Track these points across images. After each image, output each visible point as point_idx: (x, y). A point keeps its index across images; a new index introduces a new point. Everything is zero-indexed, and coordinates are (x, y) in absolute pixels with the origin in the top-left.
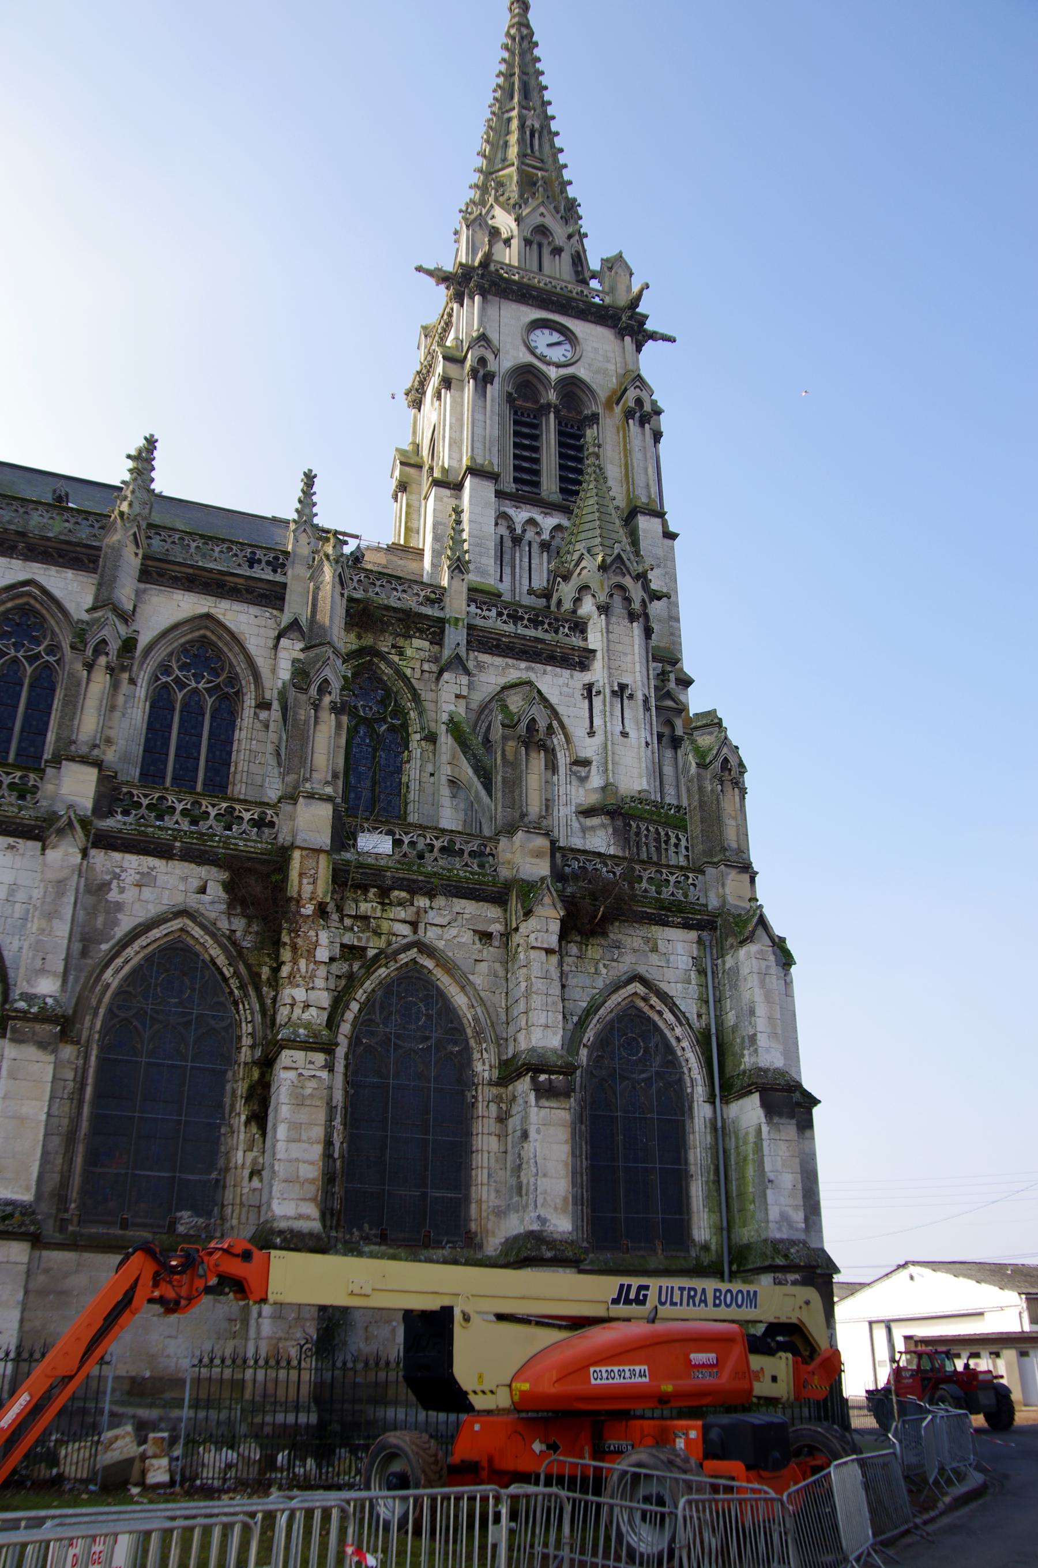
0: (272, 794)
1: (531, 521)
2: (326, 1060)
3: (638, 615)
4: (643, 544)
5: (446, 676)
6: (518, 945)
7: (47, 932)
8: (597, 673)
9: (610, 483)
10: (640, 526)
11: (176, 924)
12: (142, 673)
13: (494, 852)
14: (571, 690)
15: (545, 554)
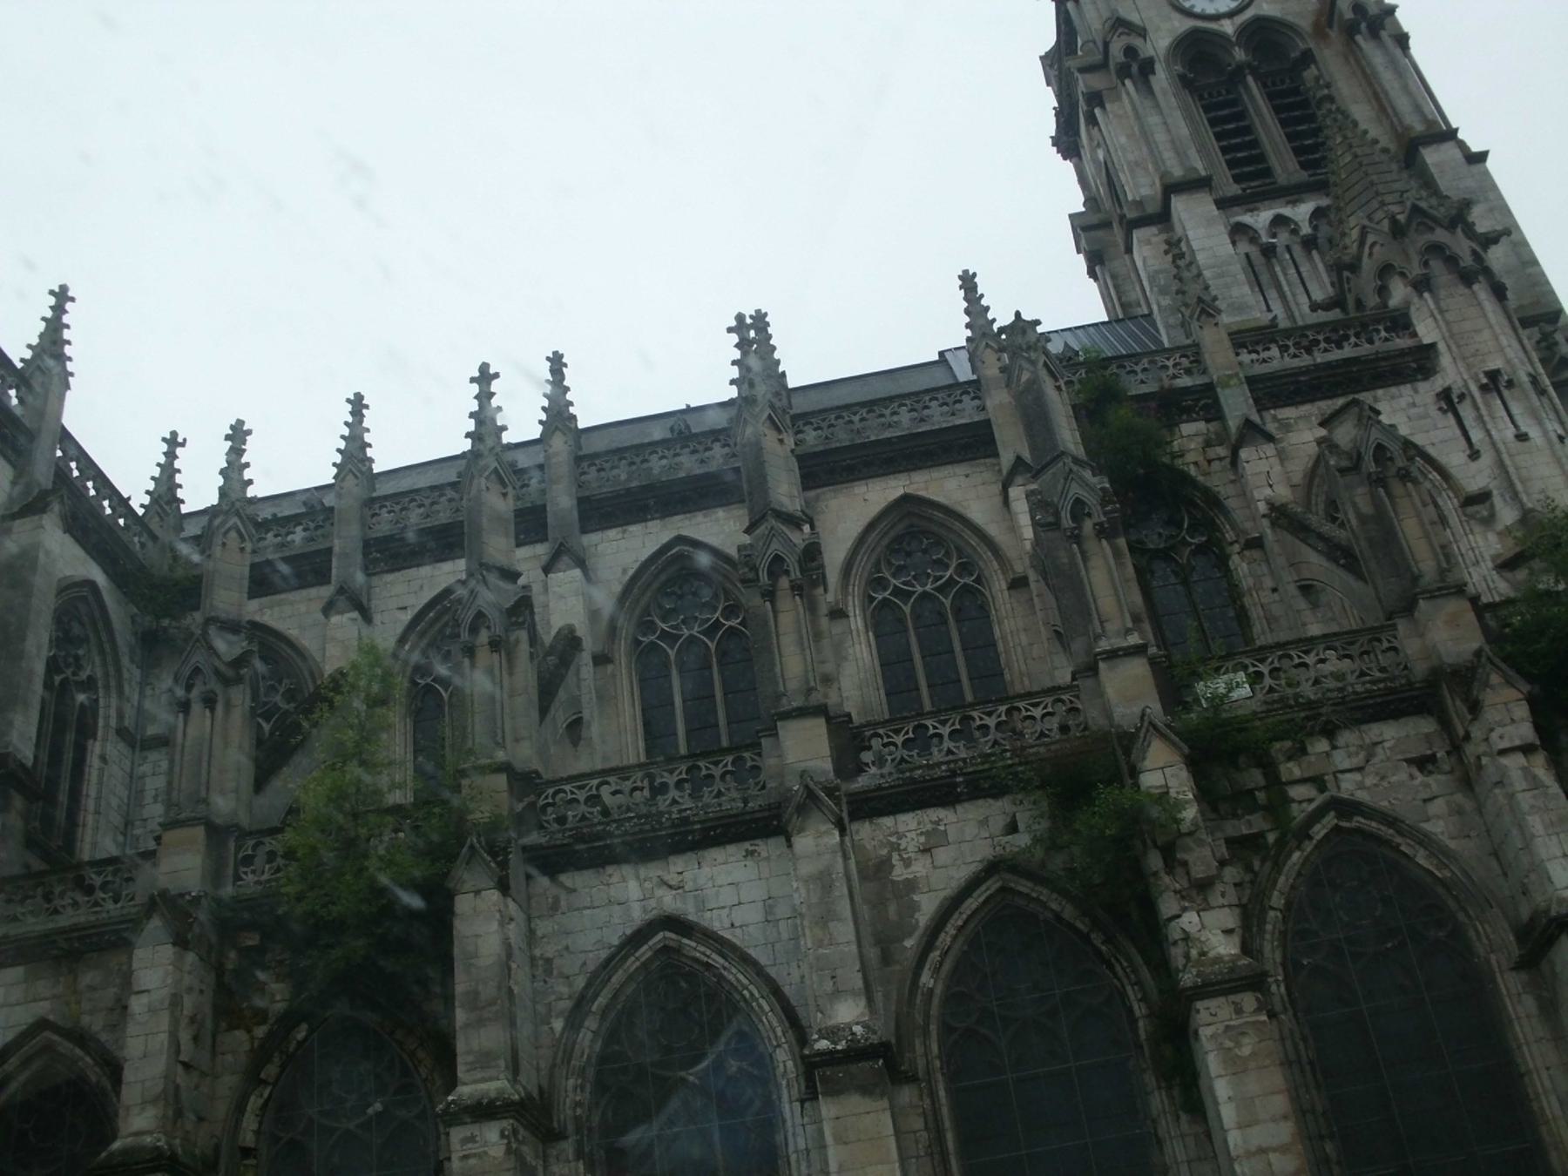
0: (1064, 676)
1: (1279, 221)
2: (1257, 999)
3: (1473, 273)
5: (1244, 454)
6: (1479, 758)
7: (826, 942)
8: (1450, 373)
9: (1363, 126)
11: (992, 886)
12: (850, 598)
13: (1396, 644)
14: (1421, 410)
15: (1314, 252)
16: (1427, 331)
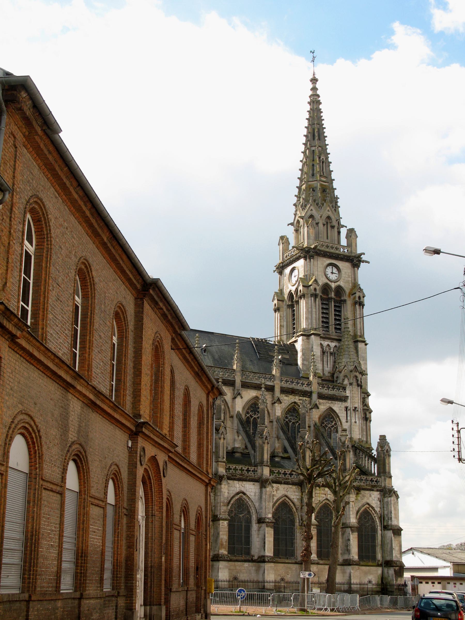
1: (328, 345)
4: (360, 353)
8: (348, 404)
16: (348, 393)
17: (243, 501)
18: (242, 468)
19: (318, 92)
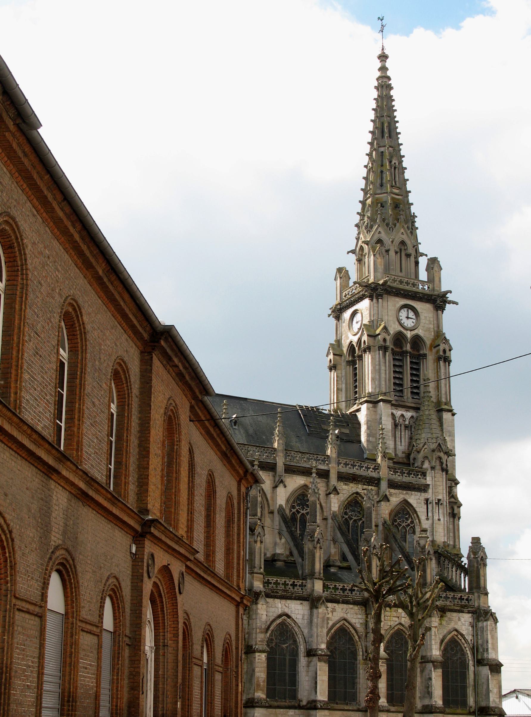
1: (402, 415)
8: (429, 495)
10: (444, 417)
16: (429, 480)
17: (287, 626)
18: (285, 582)
19: (389, 73)
